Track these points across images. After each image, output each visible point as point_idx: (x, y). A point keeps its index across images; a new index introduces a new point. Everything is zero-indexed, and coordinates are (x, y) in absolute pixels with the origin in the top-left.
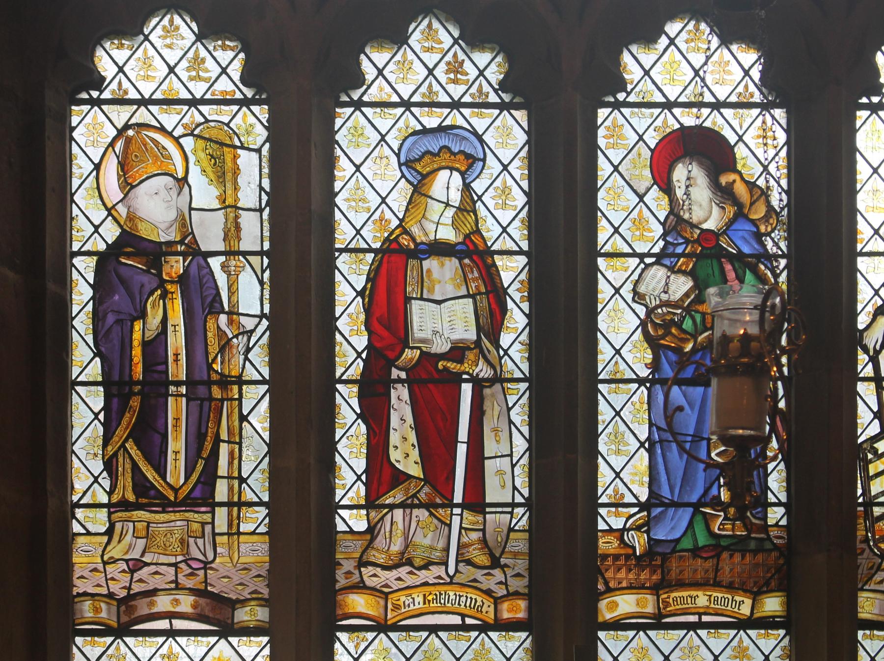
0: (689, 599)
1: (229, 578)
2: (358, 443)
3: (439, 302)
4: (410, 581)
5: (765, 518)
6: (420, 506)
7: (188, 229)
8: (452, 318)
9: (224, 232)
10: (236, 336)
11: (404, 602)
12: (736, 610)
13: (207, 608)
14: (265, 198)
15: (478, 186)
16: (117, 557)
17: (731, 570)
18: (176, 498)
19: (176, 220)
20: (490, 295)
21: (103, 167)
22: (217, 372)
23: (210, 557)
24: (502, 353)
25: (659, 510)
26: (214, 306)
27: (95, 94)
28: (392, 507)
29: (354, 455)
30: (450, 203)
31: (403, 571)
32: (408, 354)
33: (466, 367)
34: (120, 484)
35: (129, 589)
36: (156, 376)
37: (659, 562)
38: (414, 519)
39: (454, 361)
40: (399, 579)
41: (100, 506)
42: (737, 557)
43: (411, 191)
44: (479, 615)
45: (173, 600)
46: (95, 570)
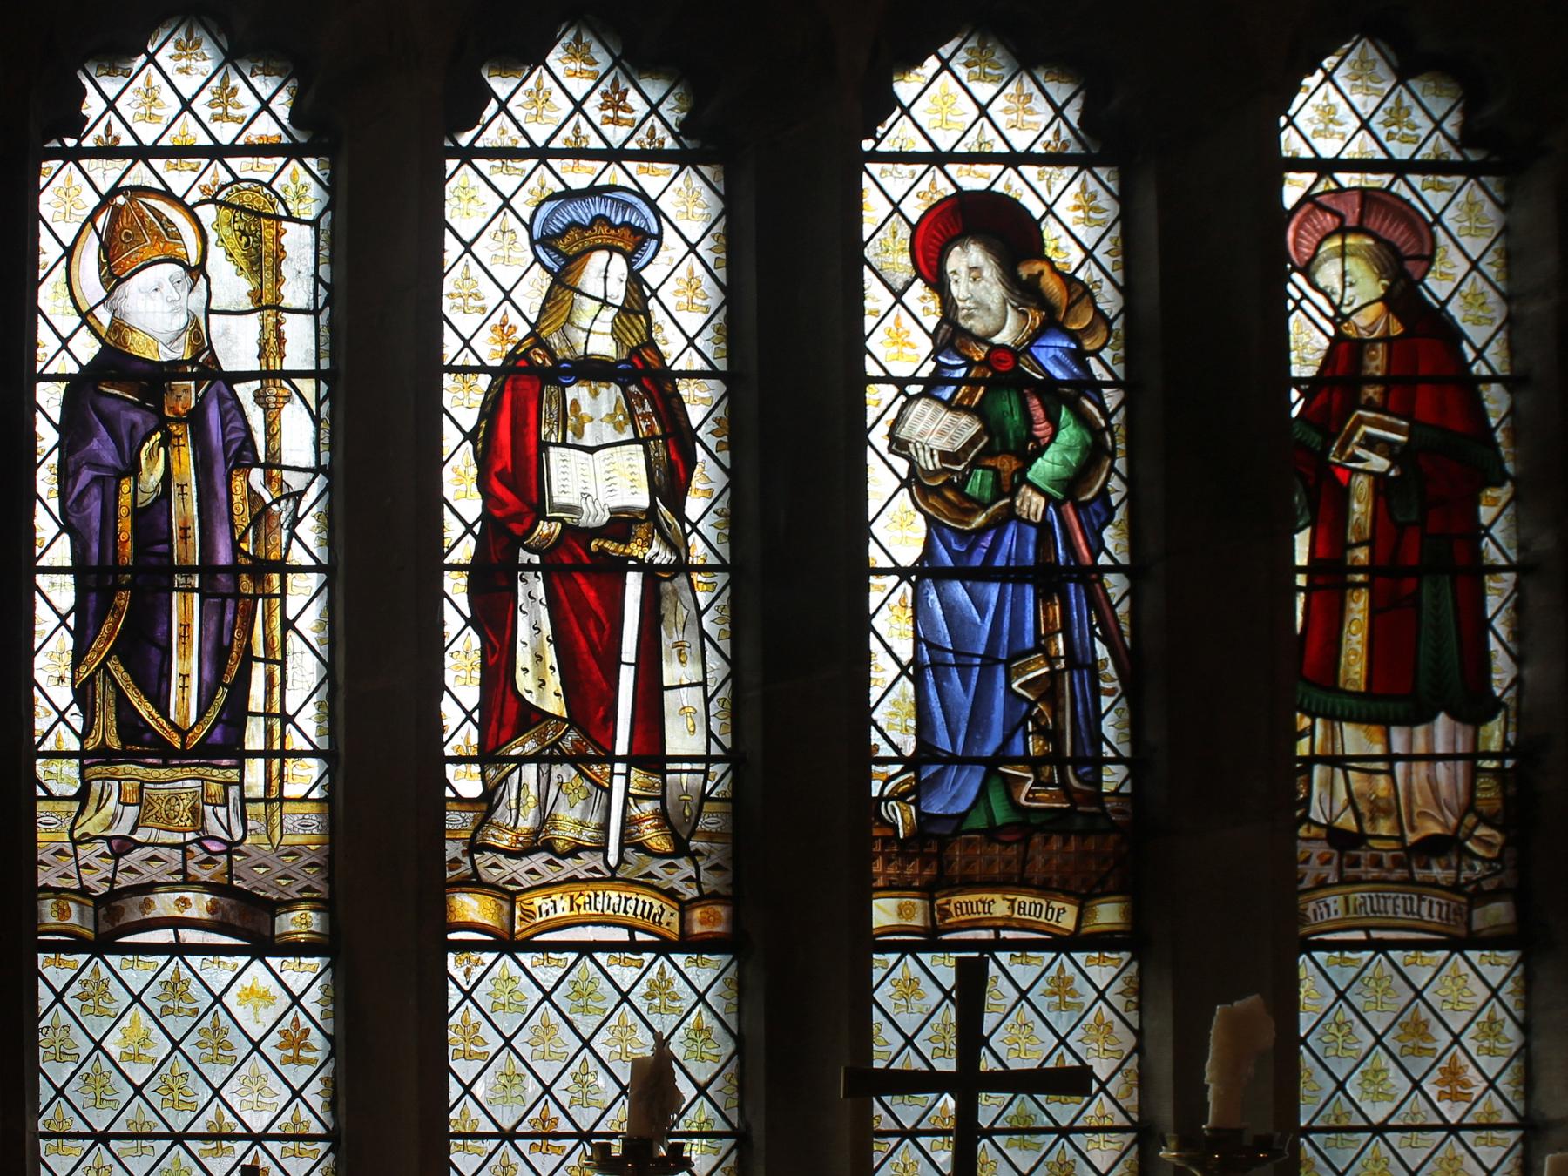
0: (980, 906)
2: (469, 663)
3: (591, 450)
4: (550, 875)
5: (1098, 782)
6: (562, 760)
8: (611, 475)
10: (277, 501)
11: (540, 907)
12: (1053, 922)
15: (652, 275)
16: (94, 833)
17: (1047, 862)
18: (183, 744)
20: (669, 441)
21: (76, 253)
22: (246, 554)
23: (238, 833)
24: (688, 528)
25: (934, 769)
26: (242, 455)
27: (70, 142)
28: (521, 760)
29: (463, 681)
30: (609, 300)
31: (538, 860)
32: (544, 528)
33: (635, 549)
35: (112, 881)
36: (153, 560)
37: (934, 849)
38: (554, 780)
39: (614, 540)
40: (532, 871)
41: (68, 755)
42: (1056, 843)
43: (549, 282)
44: (656, 928)
46: (61, 852)
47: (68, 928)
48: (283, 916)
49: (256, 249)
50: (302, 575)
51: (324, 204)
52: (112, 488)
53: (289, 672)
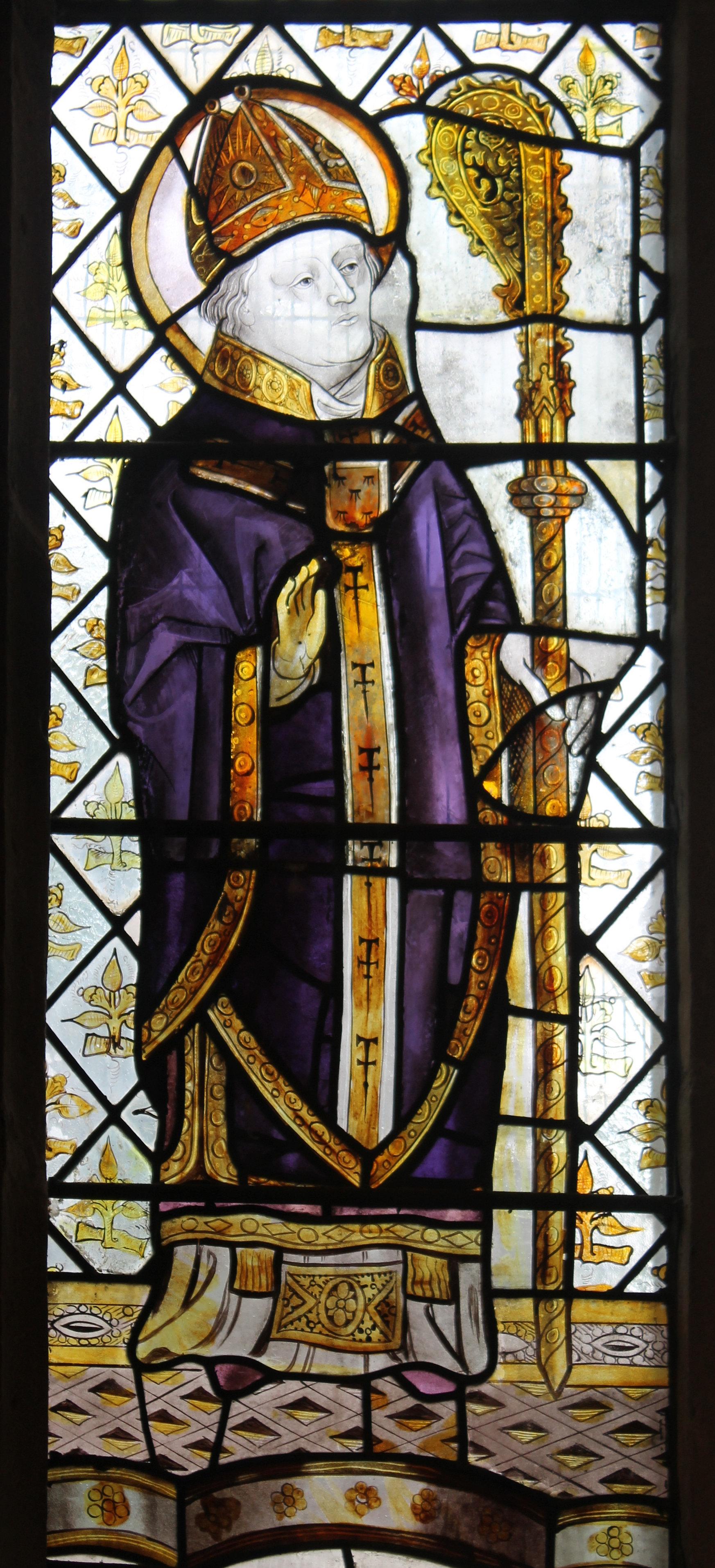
1: (536, 1428)
7: (404, 385)
9: (521, 392)
10: (559, 700)
13: (466, 1519)
14: (648, 292)
18: (366, 1176)
19: (366, 358)
21: (141, 205)
22: (496, 804)
23: (478, 1361)
34: (190, 1129)
35: (216, 1448)
36: (303, 812)
45: (356, 1490)
46: (109, 1387)
47: (124, 1540)
48: (571, 1531)
49: (510, 203)
50: (612, 847)
51: (650, 115)
52: (220, 668)
53: (585, 1039)
